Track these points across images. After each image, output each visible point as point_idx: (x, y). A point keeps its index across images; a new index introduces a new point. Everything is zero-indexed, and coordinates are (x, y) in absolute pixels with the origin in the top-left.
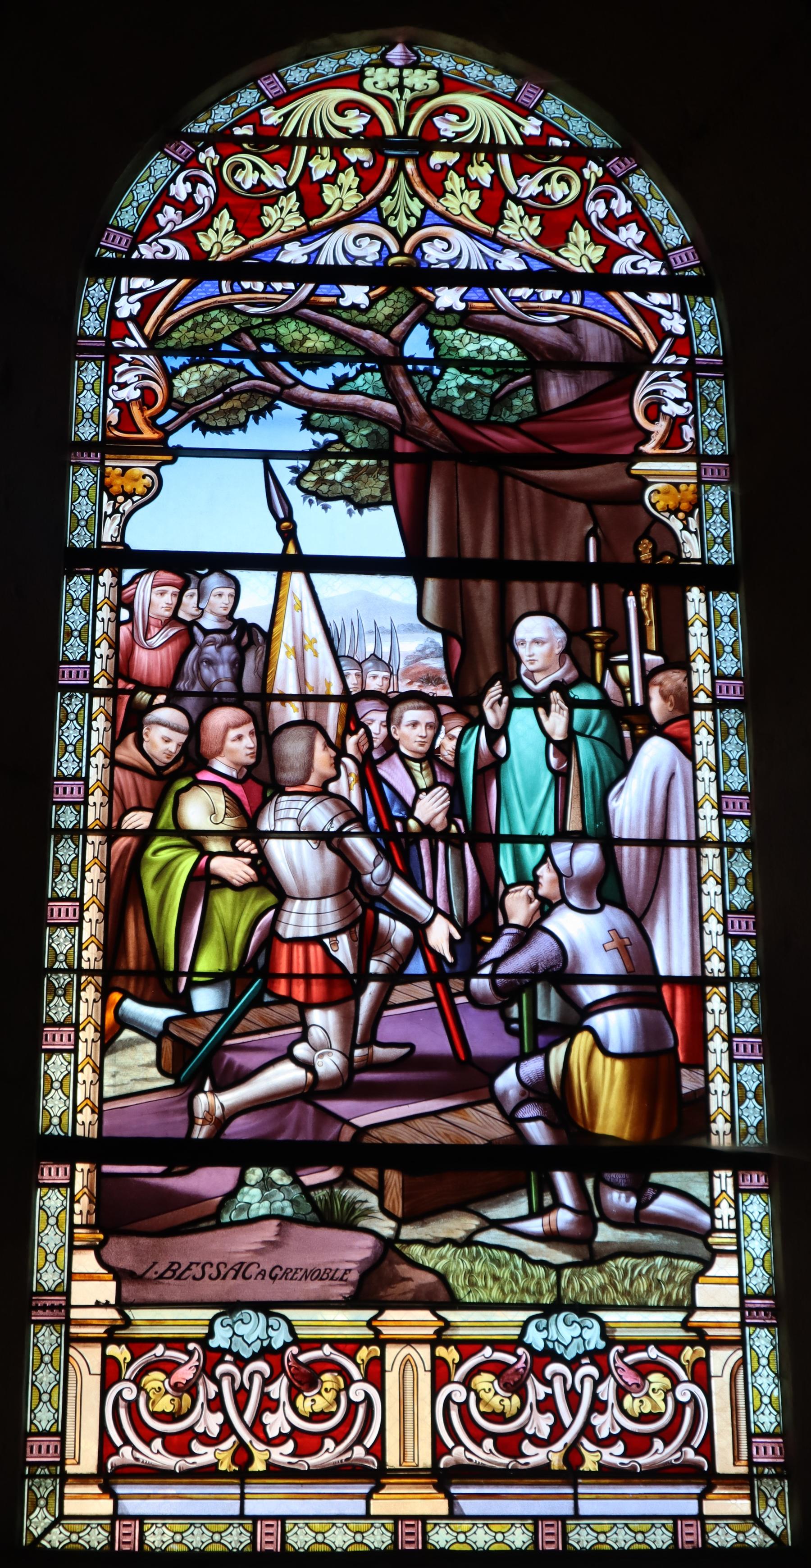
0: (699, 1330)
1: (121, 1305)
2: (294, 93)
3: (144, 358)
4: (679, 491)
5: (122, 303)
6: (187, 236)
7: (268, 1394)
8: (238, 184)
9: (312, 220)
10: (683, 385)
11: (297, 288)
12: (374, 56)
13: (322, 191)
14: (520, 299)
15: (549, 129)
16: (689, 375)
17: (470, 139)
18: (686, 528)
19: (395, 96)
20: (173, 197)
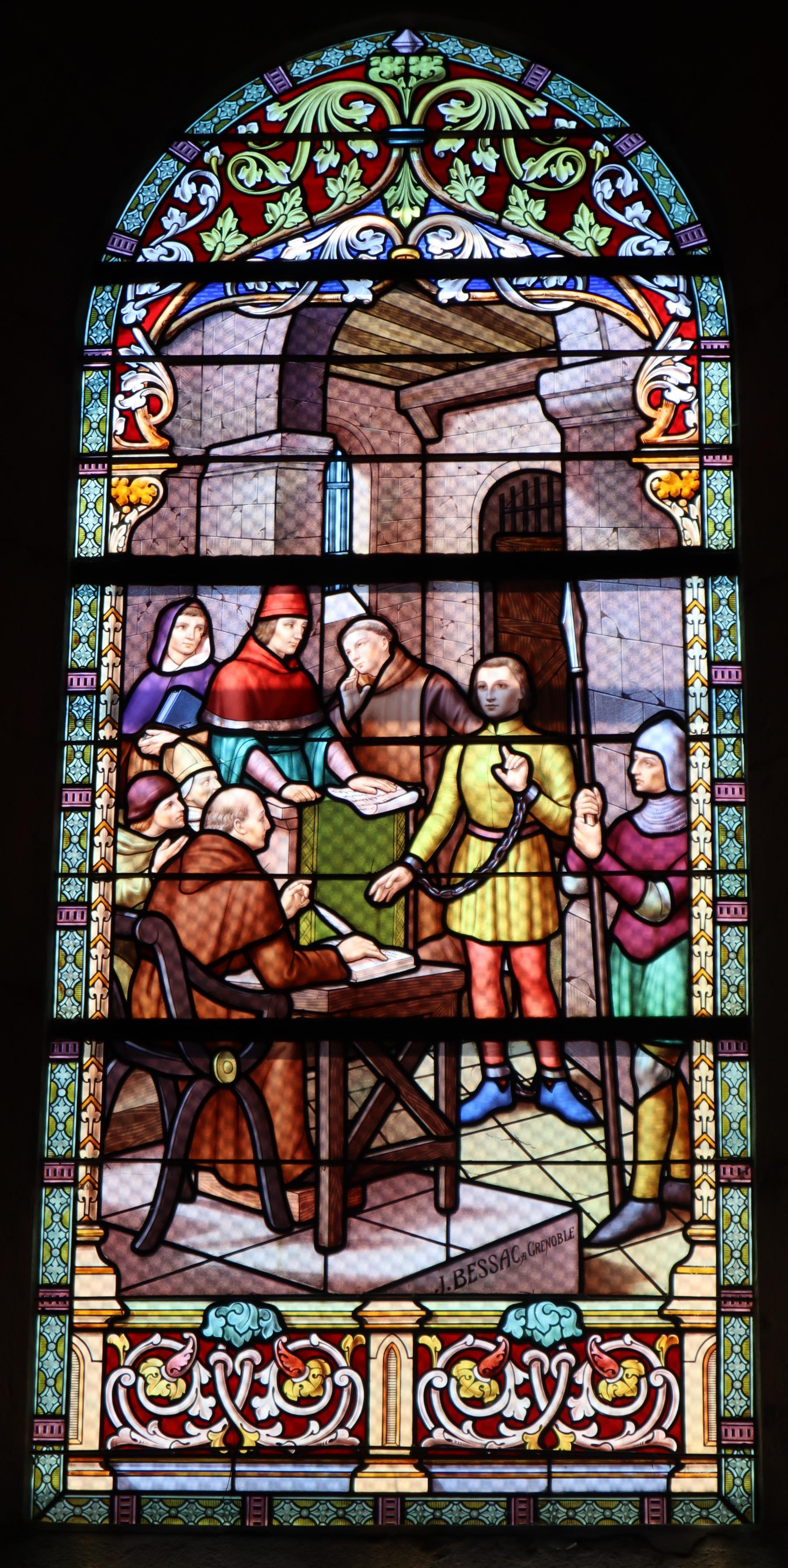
0: (676, 1319)
1: (122, 1295)
2: (299, 88)
3: (150, 365)
4: (681, 478)
5: (128, 309)
6: (190, 238)
7: (258, 1381)
8: (241, 182)
9: (316, 214)
10: (689, 369)
11: (301, 286)
12: (379, 45)
13: (326, 185)
14: (524, 287)
15: (555, 110)
16: (694, 361)
17: (472, 126)
18: (687, 515)
19: (400, 84)
20: (178, 199)
